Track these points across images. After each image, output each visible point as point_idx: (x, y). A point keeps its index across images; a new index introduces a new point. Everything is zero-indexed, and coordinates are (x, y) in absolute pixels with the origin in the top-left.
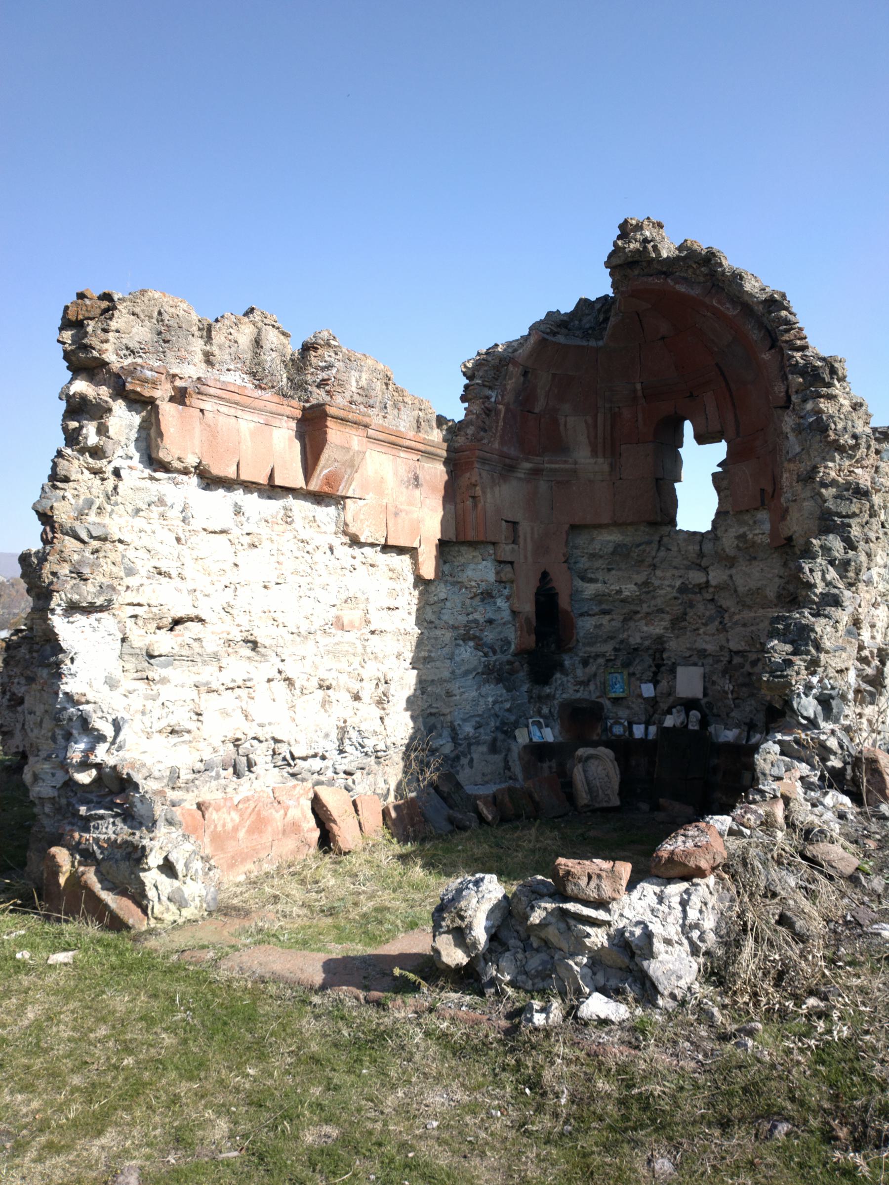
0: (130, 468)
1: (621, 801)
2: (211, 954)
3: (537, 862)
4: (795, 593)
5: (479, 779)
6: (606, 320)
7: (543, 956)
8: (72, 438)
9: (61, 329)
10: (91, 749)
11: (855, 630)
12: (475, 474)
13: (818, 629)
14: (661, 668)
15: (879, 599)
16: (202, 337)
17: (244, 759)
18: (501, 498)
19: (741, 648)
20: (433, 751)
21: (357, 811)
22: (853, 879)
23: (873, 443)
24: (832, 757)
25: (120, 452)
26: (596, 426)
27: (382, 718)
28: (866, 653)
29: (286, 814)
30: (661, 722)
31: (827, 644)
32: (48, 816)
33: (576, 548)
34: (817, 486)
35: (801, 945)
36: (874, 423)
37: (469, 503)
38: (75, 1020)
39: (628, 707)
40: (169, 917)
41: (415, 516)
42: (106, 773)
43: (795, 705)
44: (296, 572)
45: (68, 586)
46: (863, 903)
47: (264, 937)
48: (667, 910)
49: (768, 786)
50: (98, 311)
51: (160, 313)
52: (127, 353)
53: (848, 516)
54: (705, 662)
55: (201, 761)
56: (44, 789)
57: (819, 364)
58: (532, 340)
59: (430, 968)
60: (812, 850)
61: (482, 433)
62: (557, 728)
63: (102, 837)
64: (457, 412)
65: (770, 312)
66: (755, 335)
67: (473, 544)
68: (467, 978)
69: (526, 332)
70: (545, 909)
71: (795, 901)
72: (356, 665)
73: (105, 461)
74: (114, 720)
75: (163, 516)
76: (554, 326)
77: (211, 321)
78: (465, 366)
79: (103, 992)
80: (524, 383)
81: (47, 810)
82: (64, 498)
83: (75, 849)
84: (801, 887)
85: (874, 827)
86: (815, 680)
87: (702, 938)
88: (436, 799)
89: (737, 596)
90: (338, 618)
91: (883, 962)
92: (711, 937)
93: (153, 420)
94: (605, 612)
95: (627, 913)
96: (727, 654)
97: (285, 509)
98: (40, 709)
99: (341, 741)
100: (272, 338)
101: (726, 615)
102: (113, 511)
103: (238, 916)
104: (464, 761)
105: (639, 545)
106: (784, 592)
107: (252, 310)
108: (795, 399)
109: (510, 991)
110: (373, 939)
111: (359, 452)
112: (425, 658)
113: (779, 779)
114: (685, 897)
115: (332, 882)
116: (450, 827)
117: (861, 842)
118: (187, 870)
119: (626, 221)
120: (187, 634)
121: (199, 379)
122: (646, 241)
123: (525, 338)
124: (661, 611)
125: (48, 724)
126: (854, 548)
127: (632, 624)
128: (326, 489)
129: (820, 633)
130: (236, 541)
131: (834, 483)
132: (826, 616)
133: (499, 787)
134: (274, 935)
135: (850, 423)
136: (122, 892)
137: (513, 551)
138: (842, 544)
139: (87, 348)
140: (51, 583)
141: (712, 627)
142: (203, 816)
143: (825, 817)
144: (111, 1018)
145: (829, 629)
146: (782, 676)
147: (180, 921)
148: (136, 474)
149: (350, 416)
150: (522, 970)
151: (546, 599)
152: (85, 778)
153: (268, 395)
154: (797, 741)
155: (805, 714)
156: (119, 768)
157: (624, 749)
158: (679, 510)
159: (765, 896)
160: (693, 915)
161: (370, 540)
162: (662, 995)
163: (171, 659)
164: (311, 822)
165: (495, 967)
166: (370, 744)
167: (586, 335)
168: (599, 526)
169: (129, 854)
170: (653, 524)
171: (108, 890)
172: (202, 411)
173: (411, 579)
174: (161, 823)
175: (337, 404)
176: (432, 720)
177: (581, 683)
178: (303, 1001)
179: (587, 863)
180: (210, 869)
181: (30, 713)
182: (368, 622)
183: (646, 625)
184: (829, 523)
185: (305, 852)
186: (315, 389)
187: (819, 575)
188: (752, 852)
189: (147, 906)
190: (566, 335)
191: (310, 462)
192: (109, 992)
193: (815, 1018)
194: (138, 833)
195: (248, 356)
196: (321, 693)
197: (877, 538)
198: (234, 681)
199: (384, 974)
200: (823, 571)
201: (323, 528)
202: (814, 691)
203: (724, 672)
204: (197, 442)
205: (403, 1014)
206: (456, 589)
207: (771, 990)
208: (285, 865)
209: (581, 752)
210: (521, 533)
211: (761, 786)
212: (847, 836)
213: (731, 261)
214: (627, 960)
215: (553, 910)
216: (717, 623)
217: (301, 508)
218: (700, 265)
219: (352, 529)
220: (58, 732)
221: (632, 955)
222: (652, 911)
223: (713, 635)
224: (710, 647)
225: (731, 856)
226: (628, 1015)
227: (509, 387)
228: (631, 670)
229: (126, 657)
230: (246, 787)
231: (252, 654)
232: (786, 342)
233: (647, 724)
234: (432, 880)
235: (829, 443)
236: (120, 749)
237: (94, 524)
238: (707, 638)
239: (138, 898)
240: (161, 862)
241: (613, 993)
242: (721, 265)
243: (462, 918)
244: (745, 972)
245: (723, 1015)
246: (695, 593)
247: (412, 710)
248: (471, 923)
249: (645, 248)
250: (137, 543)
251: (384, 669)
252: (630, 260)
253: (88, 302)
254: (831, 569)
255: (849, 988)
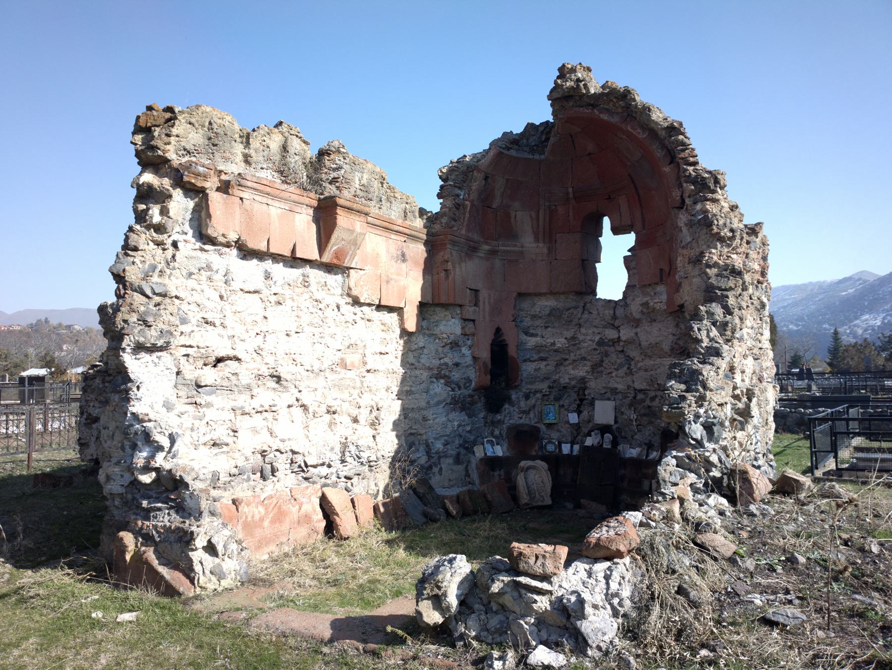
0: (185, 241)
1: (552, 500)
2: (244, 615)
3: (491, 546)
4: (686, 346)
5: (447, 484)
6: (547, 139)
7: (500, 617)
8: (141, 217)
9: (134, 133)
10: (152, 457)
11: (731, 375)
12: (448, 253)
13: (705, 373)
14: (583, 401)
15: (747, 352)
16: (242, 143)
17: (269, 466)
18: (467, 271)
19: (643, 388)
20: (412, 462)
21: (354, 507)
22: (732, 561)
23: (745, 235)
24: (714, 469)
25: (177, 229)
26: (538, 219)
27: (374, 437)
28: (738, 392)
29: (300, 509)
30: (583, 442)
31: (711, 384)
32: (117, 508)
33: (522, 310)
34: (703, 266)
35: (695, 610)
36: (746, 222)
37: (443, 274)
38: (138, 665)
39: (559, 431)
40: (211, 587)
41: (402, 283)
42: (163, 476)
43: (687, 430)
44: (311, 324)
45: (136, 331)
46: (739, 579)
47: (284, 602)
48: (594, 583)
49: (668, 490)
50: (163, 120)
51: (210, 123)
52: (185, 153)
53: (726, 290)
54: (617, 397)
55: (236, 467)
56: (114, 488)
57: (707, 175)
58: (492, 153)
59: (414, 626)
60: (701, 538)
61: (453, 222)
62: (505, 448)
63: (160, 524)
64: (434, 206)
65: (671, 136)
66: (659, 153)
67: (445, 306)
68: (442, 634)
69: (487, 147)
70: (503, 581)
71: (690, 577)
72: (355, 396)
73: (166, 236)
74: (170, 435)
75: (210, 279)
76: (508, 144)
77: (249, 130)
78: (441, 171)
79: (160, 644)
80: (485, 186)
81: (116, 503)
82: (133, 263)
83: (137, 533)
84: (693, 566)
85: (746, 522)
86: (702, 411)
87: (621, 604)
88: (414, 498)
89: (641, 348)
90: (342, 359)
91: (756, 623)
92: (628, 603)
93: (204, 205)
94: (542, 359)
95: (564, 585)
96: (632, 392)
97: (304, 275)
98: (112, 426)
99: (343, 453)
100: (295, 145)
101: (633, 363)
102: (171, 274)
103: (264, 586)
104: (435, 470)
105: (568, 309)
106: (676, 346)
107: (281, 123)
108: (687, 201)
109: (475, 644)
110: (368, 604)
111: (361, 234)
112: (407, 392)
113: (676, 484)
114: (608, 572)
115: (336, 560)
116: (424, 520)
117: (736, 532)
118: (225, 550)
119: (564, 65)
120: (228, 370)
121: (239, 174)
122: (578, 80)
123: (486, 152)
124: (584, 359)
125: (118, 437)
126: (731, 314)
127: (562, 368)
128: (335, 261)
129: (706, 376)
130: (266, 299)
131: (716, 265)
132: (710, 364)
133: (461, 489)
134: (292, 601)
135: (728, 221)
136: (175, 566)
137: (475, 311)
138: (722, 310)
139: (154, 148)
140: (123, 328)
141: (622, 372)
142: (237, 509)
143: (709, 514)
144: (166, 663)
145: (712, 373)
146: (678, 408)
147: (220, 589)
148: (190, 246)
149: (355, 206)
150: (484, 628)
151: (499, 348)
152: (147, 479)
153: (292, 188)
154: (689, 457)
155: (694, 436)
156: (174, 471)
157: (555, 462)
158: (598, 283)
159: (667, 572)
160: (614, 586)
161: (368, 301)
162: (591, 647)
163: (215, 388)
164: (320, 515)
165: (464, 625)
166: (364, 456)
167: (532, 151)
168: (539, 295)
169: (181, 537)
170: (579, 294)
171: (164, 565)
172: (241, 199)
173: (398, 331)
174: (205, 514)
175: (345, 197)
176: (412, 438)
177: (524, 412)
178: (316, 651)
179: (535, 546)
180: (242, 550)
181: (104, 428)
182: (365, 363)
183: (573, 369)
184: (712, 294)
185: (314, 537)
186: (328, 185)
187: (705, 333)
188: (658, 539)
189: (194, 578)
190: (517, 150)
191: (323, 240)
192: (165, 644)
193: (706, 665)
194: (187, 522)
195: (277, 158)
196: (328, 417)
197: (748, 306)
198: (262, 406)
199: (378, 631)
200: (707, 330)
201: (332, 291)
202: (701, 419)
203: (631, 405)
204: (237, 222)
205: (393, 661)
206: (431, 340)
207: (673, 643)
208: (299, 547)
209: (523, 464)
210: (481, 298)
211: (663, 490)
212: (726, 528)
213: (642, 97)
214: (564, 621)
215: (509, 582)
216: (625, 368)
217: (316, 275)
218: (619, 100)
219: (354, 292)
220: (127, 443)
221: (569, 617)
222: (584, 583)
223: (623, 377)
224: (620, 387)
225: (643, 542)
226: (565, 662)
227: (474, 188)
228: (561, 403)
229: (180, 387)
230: (270, 488)
231: (277, 386)
232: (682, 159)
233: (573, 443)
234: (412, 559)
235: (712, 234)
236: (174, 457)
237: (157, 283)
238: (618, 380)
239: (187, 572)
240: (205, 544)
241: (554, 645)
242: (634, 100)
243: (439, 588)
244: (654, 630)
245: (637, 662)
246: (610, 346)
247: (397, 431)
248: (446, 591)
249: (578, 86)
250: (190, 299)
251: (376, 399)
252: (566, 94)
253: (155, 113)
254: (713, 328)
255: (731, 642)
